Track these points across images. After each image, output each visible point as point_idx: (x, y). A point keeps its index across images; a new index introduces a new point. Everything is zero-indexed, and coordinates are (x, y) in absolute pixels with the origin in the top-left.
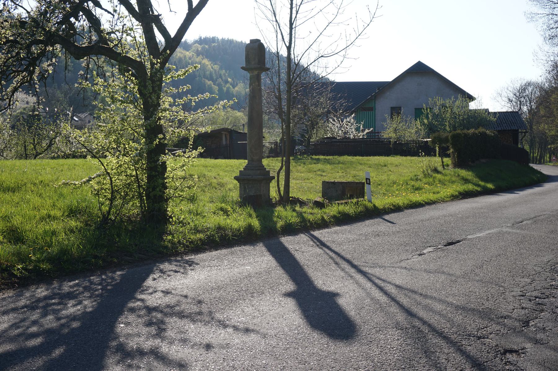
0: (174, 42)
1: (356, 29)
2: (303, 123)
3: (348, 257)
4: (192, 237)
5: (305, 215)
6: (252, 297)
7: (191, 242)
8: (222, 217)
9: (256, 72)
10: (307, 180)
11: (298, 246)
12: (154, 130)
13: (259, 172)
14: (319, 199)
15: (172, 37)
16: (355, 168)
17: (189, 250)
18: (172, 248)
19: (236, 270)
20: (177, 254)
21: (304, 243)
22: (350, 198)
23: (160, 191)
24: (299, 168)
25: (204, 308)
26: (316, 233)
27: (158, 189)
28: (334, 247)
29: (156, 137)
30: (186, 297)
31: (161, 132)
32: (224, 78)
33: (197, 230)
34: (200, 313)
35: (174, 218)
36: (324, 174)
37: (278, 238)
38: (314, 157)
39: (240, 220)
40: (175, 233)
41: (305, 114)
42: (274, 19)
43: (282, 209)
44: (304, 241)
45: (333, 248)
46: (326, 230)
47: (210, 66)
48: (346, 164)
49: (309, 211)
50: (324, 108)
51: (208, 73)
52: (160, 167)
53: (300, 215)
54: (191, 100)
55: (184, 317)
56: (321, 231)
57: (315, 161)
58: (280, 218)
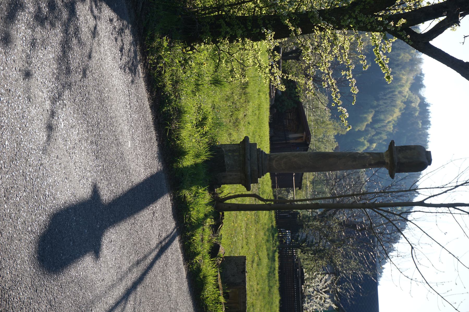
0: (423, 44)
1: (450, 293)
2: (321, 239)
3: (147, 280)
4: (166, 75)
5: (200, 230)
6: (92, 142)
7: (160, 74)
8: (194, 118)
9: (387, 160)
10: (247, 234)
11: (158, 218)
12: (306, 22)
13: (256, 168)
14: (223, 251)
15: (431, 42)
16: (264, 307)
17: (150, 70)
18: (152, 48)
19: (126, 127)
20: (145, 54)
21: (164, 225)
22: (224, 293)
23: (227, 33)
24: (262, 233)
25: (76, 77)
26: (176, 244)
27: (228, 30)
28: (159, 264)
29: (297, 25)
30: (90, 57)
31: (305, 32)
32: (376, 138)
33: (176, 83)
34: (69, 71)
35: (191, 52)
36: (255, 265)
37: (168, 192)
38: (277, 255)
39: (192, 143)
40: (171, 54)
41: (333, 241)
42: (459, 184)
43: (207, 201)
44: (166, 225)
45: (157, 262)
46: (181, 259)
47: (391, 118)
48: (269, 296)
49: (206, 238)
50: (342, 267)
51: (382, 117)
52: (258, 30)
53: (200, 223)
54: (348, 69)
55: (63, 47)
56: (180, 250)
57: (271, 255)
58: (195, 196)
